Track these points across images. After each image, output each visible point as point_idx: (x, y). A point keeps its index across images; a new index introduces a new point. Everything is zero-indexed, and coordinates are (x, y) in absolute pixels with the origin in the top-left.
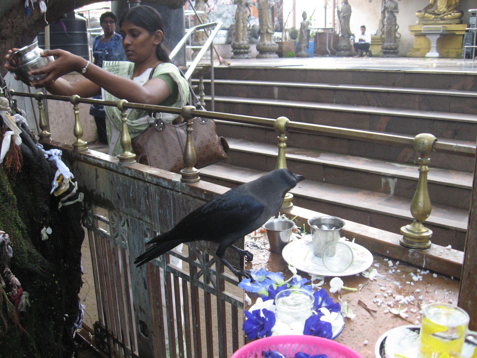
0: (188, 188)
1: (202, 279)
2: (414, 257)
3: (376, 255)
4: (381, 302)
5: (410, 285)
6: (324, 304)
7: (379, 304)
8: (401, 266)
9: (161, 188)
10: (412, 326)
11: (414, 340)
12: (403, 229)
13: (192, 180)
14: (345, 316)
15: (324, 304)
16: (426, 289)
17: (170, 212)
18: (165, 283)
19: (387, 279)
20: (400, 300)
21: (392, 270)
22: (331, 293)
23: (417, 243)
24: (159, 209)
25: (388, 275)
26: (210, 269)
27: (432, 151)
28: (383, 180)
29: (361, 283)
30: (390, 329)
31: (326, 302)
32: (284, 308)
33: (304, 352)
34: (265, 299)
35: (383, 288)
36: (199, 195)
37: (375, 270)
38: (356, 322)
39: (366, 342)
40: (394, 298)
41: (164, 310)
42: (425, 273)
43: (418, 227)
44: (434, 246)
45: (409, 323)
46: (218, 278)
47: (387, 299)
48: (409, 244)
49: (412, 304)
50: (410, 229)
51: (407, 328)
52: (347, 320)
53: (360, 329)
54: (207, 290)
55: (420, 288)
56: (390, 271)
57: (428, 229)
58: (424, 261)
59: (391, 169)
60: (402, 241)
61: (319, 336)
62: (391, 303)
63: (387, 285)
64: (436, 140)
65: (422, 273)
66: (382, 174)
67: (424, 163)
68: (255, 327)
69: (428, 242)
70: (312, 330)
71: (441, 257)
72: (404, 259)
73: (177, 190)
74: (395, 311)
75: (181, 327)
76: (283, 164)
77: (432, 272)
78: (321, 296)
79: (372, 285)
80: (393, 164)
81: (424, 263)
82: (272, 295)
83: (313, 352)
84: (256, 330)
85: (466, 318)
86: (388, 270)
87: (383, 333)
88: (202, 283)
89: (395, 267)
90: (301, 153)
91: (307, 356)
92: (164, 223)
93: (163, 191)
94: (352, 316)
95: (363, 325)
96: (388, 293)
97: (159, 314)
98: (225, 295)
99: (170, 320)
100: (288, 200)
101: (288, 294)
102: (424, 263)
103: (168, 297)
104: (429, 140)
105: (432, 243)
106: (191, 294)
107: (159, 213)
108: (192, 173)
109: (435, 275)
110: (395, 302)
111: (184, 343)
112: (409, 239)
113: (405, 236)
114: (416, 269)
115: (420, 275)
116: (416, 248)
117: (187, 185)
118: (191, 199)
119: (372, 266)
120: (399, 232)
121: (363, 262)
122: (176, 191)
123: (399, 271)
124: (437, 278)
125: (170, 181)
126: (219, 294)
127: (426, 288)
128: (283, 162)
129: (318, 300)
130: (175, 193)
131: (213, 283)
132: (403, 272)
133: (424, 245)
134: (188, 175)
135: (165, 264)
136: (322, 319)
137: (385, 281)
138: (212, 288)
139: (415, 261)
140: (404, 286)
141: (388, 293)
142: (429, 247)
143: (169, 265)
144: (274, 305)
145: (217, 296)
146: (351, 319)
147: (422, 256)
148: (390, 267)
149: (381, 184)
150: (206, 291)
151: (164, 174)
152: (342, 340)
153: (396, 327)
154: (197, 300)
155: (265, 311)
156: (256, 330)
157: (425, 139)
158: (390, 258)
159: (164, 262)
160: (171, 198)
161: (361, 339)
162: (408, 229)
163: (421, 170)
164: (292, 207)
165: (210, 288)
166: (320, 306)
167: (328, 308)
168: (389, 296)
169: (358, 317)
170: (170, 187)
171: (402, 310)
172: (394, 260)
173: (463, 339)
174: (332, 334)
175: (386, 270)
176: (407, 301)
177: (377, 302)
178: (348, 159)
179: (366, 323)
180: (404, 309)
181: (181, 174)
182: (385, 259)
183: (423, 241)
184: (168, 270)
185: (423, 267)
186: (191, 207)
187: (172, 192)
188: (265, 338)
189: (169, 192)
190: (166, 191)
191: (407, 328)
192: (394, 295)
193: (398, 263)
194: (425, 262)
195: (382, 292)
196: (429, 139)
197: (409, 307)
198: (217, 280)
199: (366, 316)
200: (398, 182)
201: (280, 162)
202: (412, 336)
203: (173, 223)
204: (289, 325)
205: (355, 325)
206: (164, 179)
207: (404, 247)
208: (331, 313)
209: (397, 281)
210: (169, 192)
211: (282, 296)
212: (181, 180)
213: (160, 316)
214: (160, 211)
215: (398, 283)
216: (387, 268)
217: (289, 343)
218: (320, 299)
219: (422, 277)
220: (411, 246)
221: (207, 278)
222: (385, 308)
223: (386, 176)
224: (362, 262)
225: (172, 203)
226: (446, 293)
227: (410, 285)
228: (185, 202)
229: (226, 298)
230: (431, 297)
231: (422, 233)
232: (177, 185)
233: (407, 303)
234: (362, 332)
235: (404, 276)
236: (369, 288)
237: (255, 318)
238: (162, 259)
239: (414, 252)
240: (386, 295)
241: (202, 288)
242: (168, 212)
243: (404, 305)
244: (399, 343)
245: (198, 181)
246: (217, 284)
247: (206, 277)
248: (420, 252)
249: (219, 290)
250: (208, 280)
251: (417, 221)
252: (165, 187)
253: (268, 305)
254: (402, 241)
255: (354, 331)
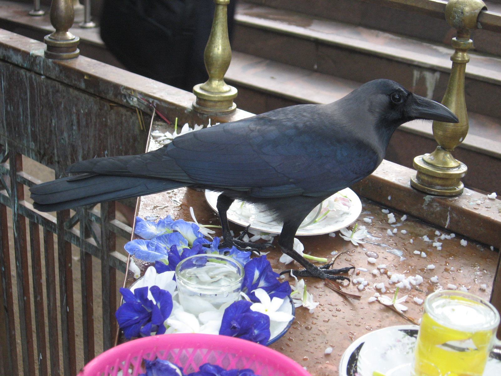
0: (57, 69)
1: (77, 230)
2: (432, 210)
3: (370, 201)
4: (366, 283)
5: (420, 256)
6: (262, 283)
7: (361, 287)
8: (409, 223)
9: (11, 66)
10: (410, 327)
11: (410, 351)
12: (418, 160)
13: (65, 55)
14: (297, 304)
15: (262, 283)
16: (446, 265)
17: (25, 110)
18: (16, 233)
19: (383, 245)
20: (398, 282)
21: (392, 229)
22: (281, 263)
23: (438, 185)
24: (7, 104)
25: (384, 237)
26: (92, 214)
27: (476, 27)
28: (416, 74)
29: (336, 250)
30: (374, 329)
31: (267, 280)
32: (193, 287)
33: (216, 364)
34: (161, 268)
35: (372, 260)
36: (76, 82)
37: (363, 228)
38: (318, 316)
39: (329, 350)
40: (389, 277)
41: (14, 281)
42: (448, 237)
43: (444, 158)
44: (469, 192)
45: (409, 322)
46: (103, 230)
47: (377, 278)
48: (425, 186)
49: (417, 290)
50: (429, 161)
51: (401, 330)
52: (301, 313)
53: (322, 329)
54: (86, 248)
55: (434, 263)
56: (389, 232)
57: (459, 162)
58: (449, 217)
59: (431, 55)
60: (415, 181)
61: (245, 338)
62: (381, 285)
63: (381, 255)
64: (485, 9)
65: (443, 237)
66: (415, 64)
67: (461, 47)
68: (137, 317)
69: (458, 185)
70: (234, 327)
71: (477, 212)
72: (415, 213)
73: (38, 71)
74: (386, 300)
75: (42, 310)
76: (222, 34)
77: (459, 236)
78: (258, 269)
79: (355, 254)
80: (435, 47)
81: (448, 220)
82: (174, 262)
83: (231, 364)
84: (138, 323)
85: (493, 318)
86: (386, 229)
87: (360, 337)
88: (77, 237)
89: (399, 225)
90: (280, 17)
91: (219, 370)
92: (15, 130)
93: (13, 72)
94: (310, 303)
95: (329, 320)
96: (379, 269)
97: (4, 287)
98: (115, 259)
99: (24, 297)
100: (227, 99)
101: (202, 262)
102: (448, 220)
103: (20, 258)
104: (472, 7)
105: (466, 186)
106: (59, 254)
107: (6, 111)
108: (65, 42)
109: (464, 243)
110: (389, 284)
111: (35, 338)
112: (426, 178)
113: (421, 172)
114: (434, 229)
115: (439, 240)
116: (436, 194)
117: (54, 63)
118: (61, 87)
119: (359, 221)
120: (410, 164)
121: (344, 213)
122: (36, 73)
123: (404, 231)
124: (466, 246)
125: (25, 54)
126: (106, 257)
127: (446, 262)
128: (223, 31)
129: (254, 275)
130: (33, 76)
131: (95, 238)
132: (411, 233)
133: (451, 190)
134: (58, 46)
135: (16, 202)
136: (255, 307)
137: (379, 247)
138: (93, 246)
139: (434, 216)
140: (408, 257)
141: (379, 269)
142: (459, 194)
143: (21, 202)
144: (174, 281)
145: (103, 259)
146: (308, 310)
147: (445, 207)
148: (389, 224)
149: (412, 80)
150: (84, 250)
151: (17, 41)
152: (288, 345)
153: (384, 327)
154: (70, 265)
155: (155, 290)
156: (138, 322)
157: (466, 6)
158: (392, 209)
159: (14, 197)
160: (27, 85)
161: (322, 346)
162: (426, 160)
163: (456, 60)
164: (234, 110)
165: (90, 245)
166: (256, 286)
167: (267, 289)
168: (381, 274)
169: (322, 308)
170: (25, 65)
171: (399, 298)
172: (398, 213)
173: (486, 352)
174: (269, 334)
175: (383, 229)
176: (410, 283)
177: (359, 283)
178: (359, 33)
179: (334, 318)
180: (402, 296)
181: (46, 42)
182: (384, 211)
183: (450, 182)
184: (20, 212)
185: (446, 227)
186: (61, 103)
187: (28, 74)
188: (154, 337)
189: (24, 73)
190: (18, 73)
191: (401, 330)
192: (389, 273)
193: (404, 218)
194: (450, 218)
195: (370, 267)
196: (473, 5)
197: (413, 293)
198: (102, 231)
199: (336, 305)
200: (440, 78)
201: (216, 29)
202: (408, 344)
203: (29, 130)
204: (197, 317)
205: (315, 321)
206: (16, 51)
207: (417, 191)
208: (271, 299)
209: (399, 249)
210: (24, 73)
211: (189, 265)
212: (46, 53)
213: (6, 289)
214: (9, 107)
215: (399, 253)
216: (385, 224)
217: (190, 347)
218: (257, 273)
219: (441, 244)
220: (428, 190)
221: (86, 228)
222: (370, 295)
223: (421, 67)
224: (341, 213)
225: (28, 94)
226: (478, 273)
227: (420, 256)
228: (51, 93)
229: (118, 263)
230: (451, 279)
231: (449, 168)
232: (37, 62)
233: (409, 287)
234: (326, 333)
235: (411, 241)
236: (349, 258)
237: (139, 301)
238: (10, 192)
239: (433, 200)
240: (375, 272)
241: (77, 245)
242: (21, 109)
243: (404, 290)
244: (384, 356)
245: (76, 56)
246: (102, 240)
247: (84, 226)
248: (443, 201)
249: (105, 249)
250: (87, 232)
251: (442, 148)
252: (17, 66)
253: (164, 281)
254: (414, 181)
255: (310, 332)
